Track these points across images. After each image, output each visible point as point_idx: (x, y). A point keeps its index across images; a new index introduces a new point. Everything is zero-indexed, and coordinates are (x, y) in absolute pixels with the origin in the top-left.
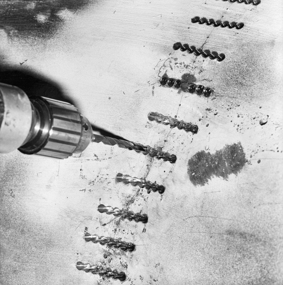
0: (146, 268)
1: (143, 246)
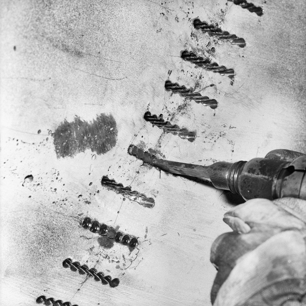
0: (171, 30)
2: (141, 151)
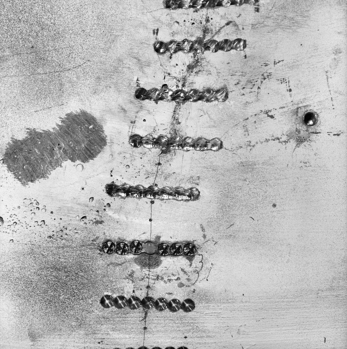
1: (152, 10)
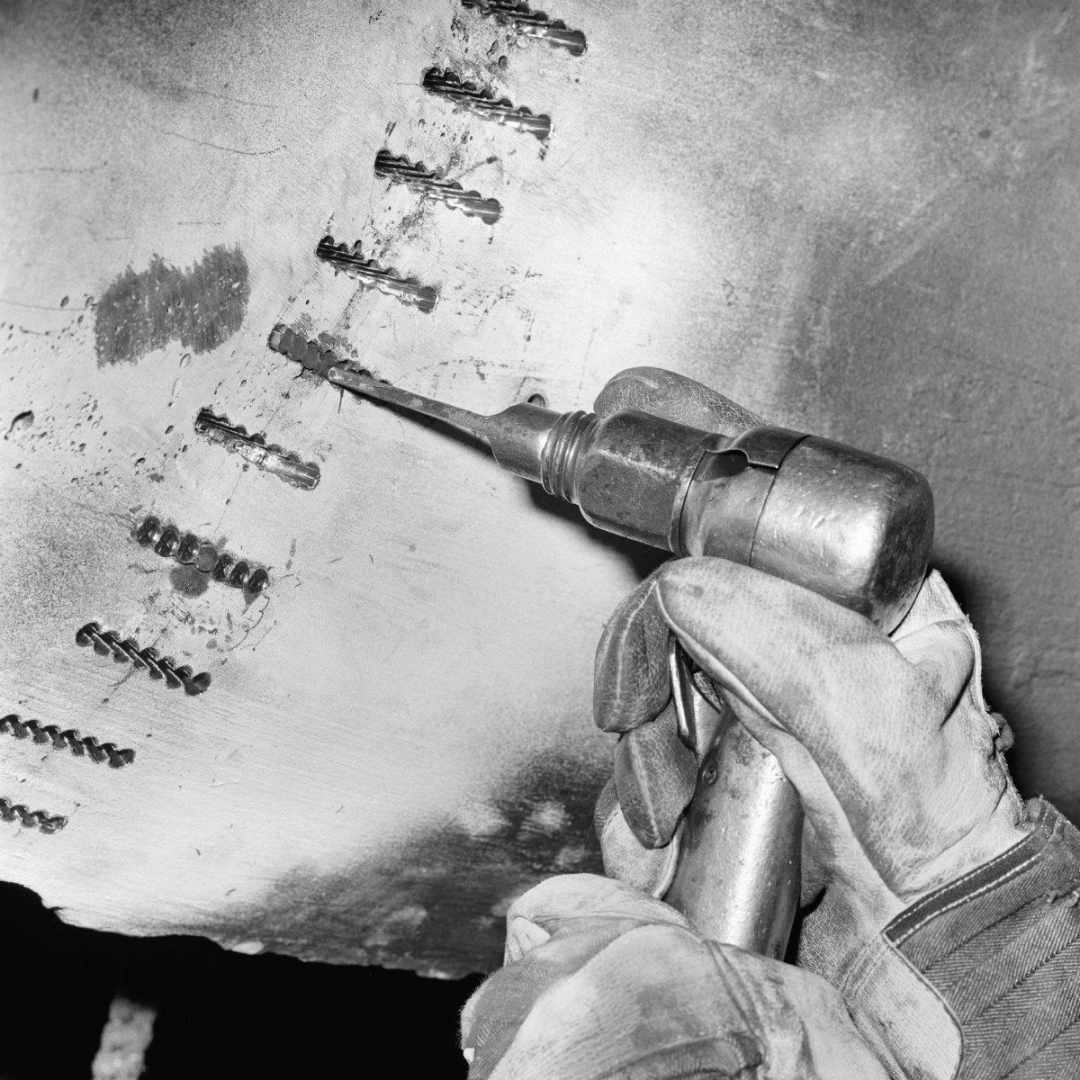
2: (300, 339)
